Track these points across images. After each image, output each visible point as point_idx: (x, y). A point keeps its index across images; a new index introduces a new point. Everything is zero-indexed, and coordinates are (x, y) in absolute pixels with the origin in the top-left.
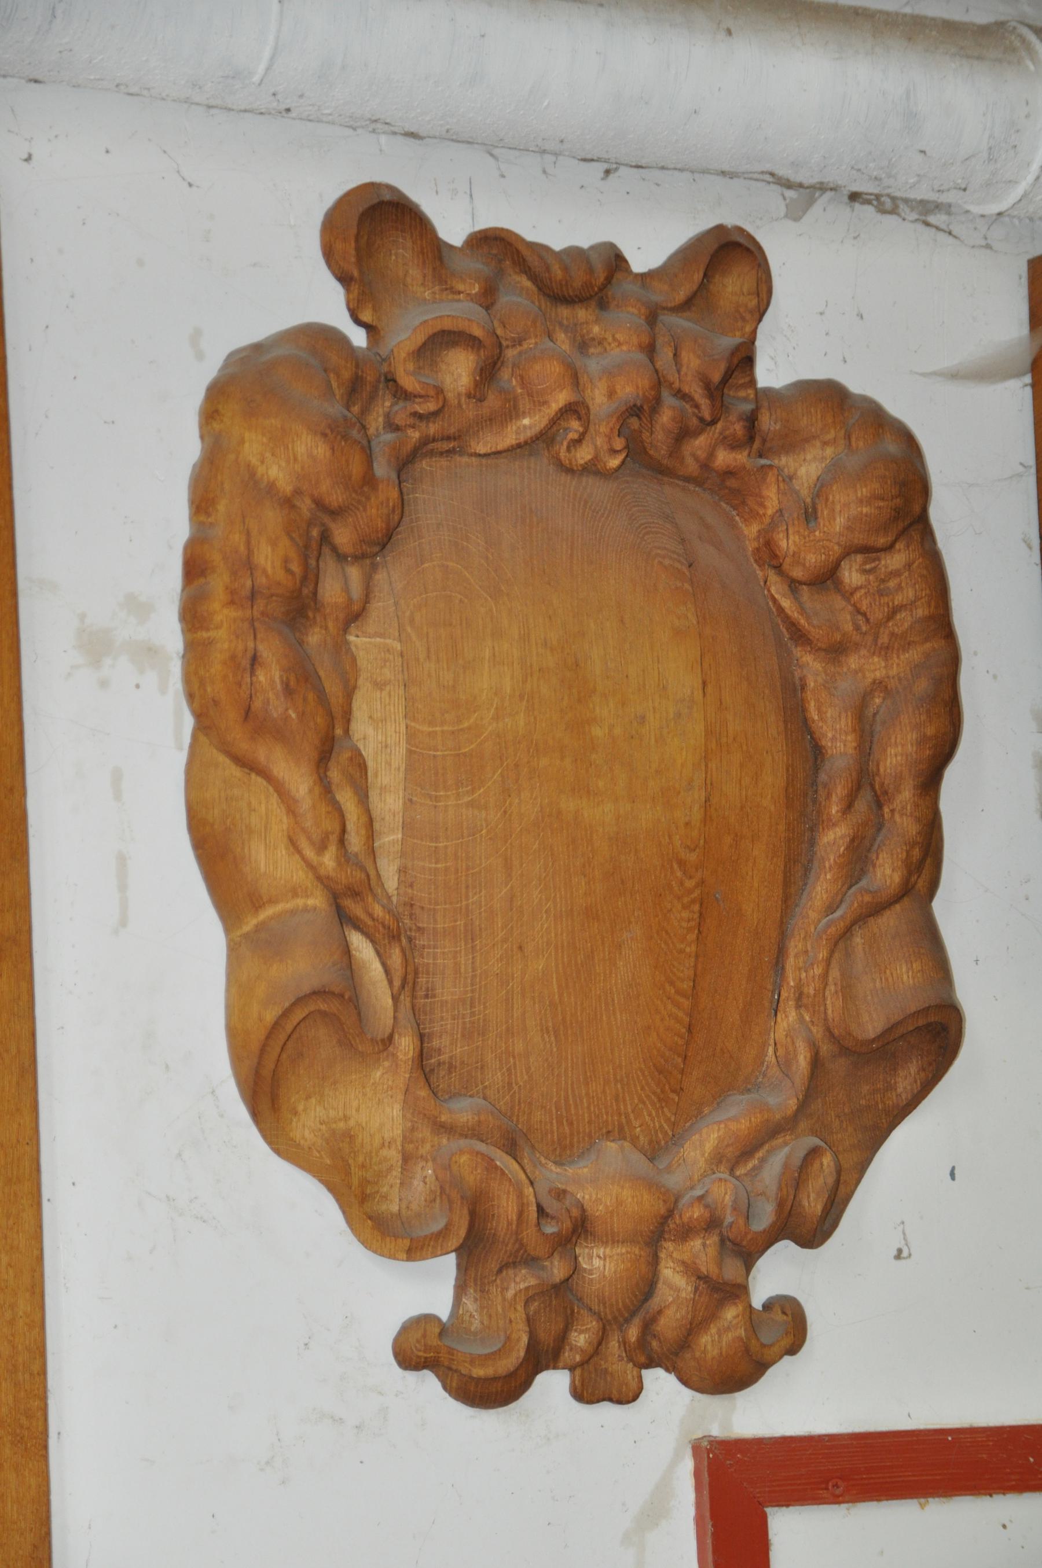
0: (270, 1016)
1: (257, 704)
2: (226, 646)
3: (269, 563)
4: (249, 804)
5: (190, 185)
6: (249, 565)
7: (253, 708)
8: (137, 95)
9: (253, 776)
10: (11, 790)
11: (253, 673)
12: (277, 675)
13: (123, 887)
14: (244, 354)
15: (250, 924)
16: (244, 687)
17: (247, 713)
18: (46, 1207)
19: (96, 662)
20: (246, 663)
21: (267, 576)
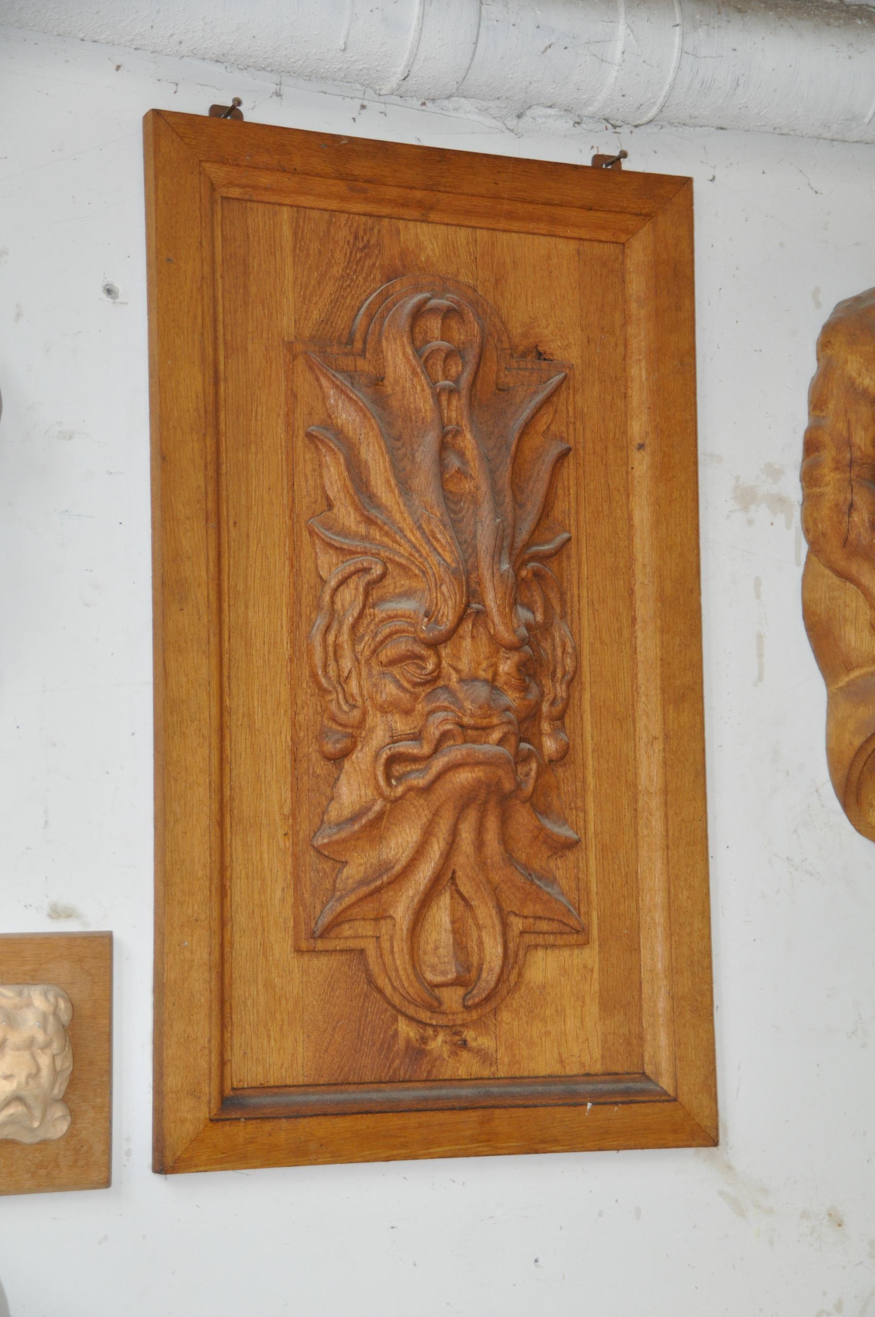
0: (858, 742)
1: (852, 536)
2: (832, 497)
3: (863, 443)
4: (845, 602)
5: (816, 193)
6: (850, 444)
7: (849, 539)
8: (787, 134)
9: (848, 583)
10: (692, 591)
11: (849, 516)
12: (866, 516)
13: (760, 655)
14: (849, 303)
15: (844, 681)
16: (844, 524)
17: (845, 542)
18: (711, 860)
19: (745, 508)
20: (845, 508)
21: (861, 451)
